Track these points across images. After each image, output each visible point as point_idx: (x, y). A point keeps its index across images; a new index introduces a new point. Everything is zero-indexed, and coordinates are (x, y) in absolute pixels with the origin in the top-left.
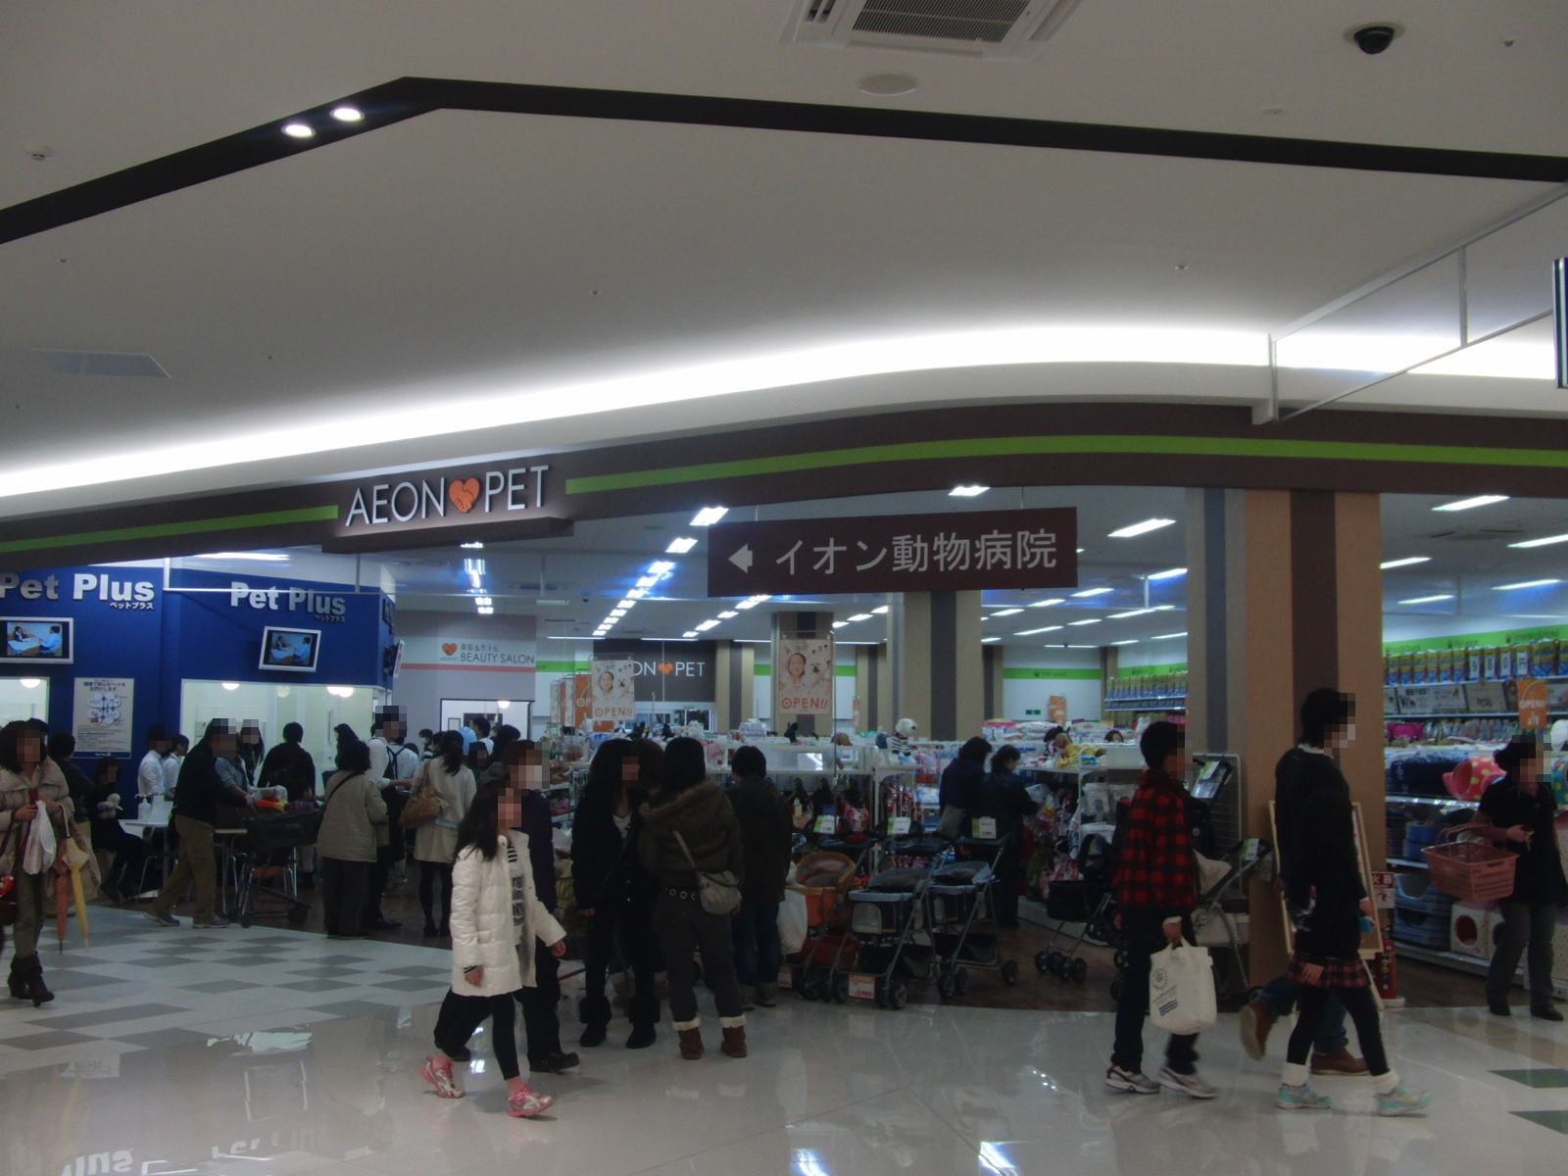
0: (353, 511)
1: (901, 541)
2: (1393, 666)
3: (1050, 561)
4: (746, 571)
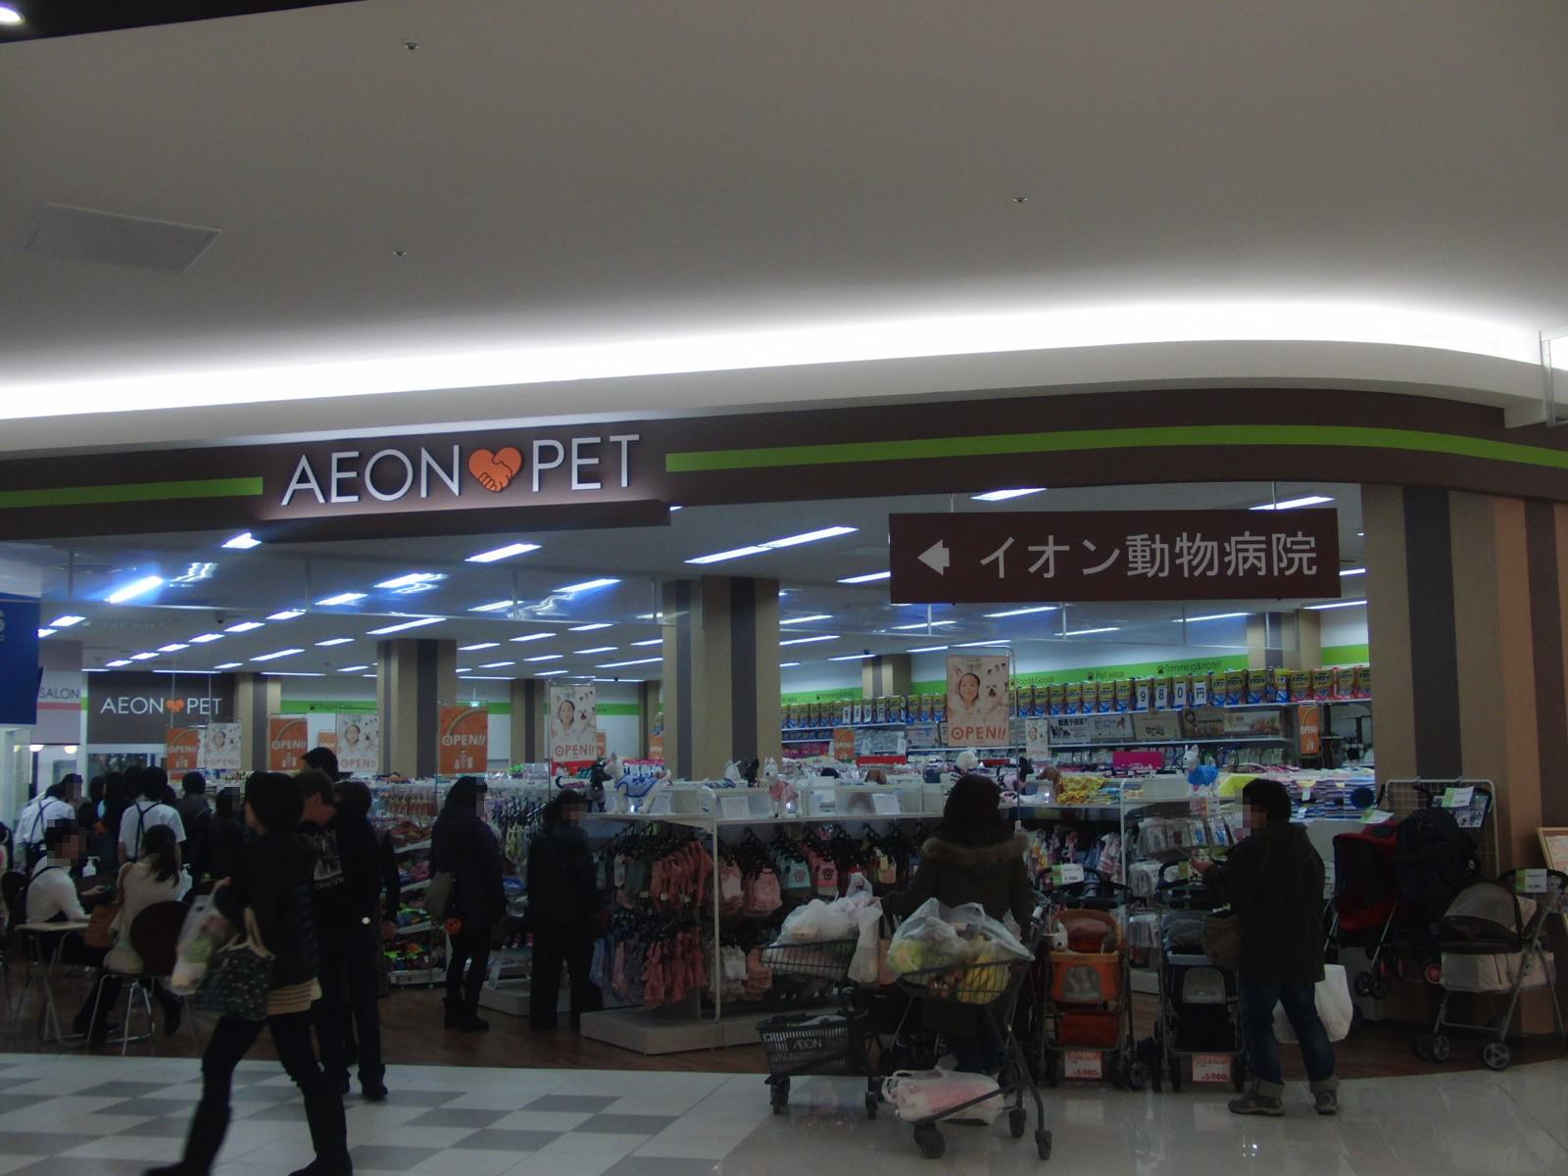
0: (294, 486)
1: (1137, 542)
2: (926, 704)
3: (1310, 568)
4: (941, 572)
